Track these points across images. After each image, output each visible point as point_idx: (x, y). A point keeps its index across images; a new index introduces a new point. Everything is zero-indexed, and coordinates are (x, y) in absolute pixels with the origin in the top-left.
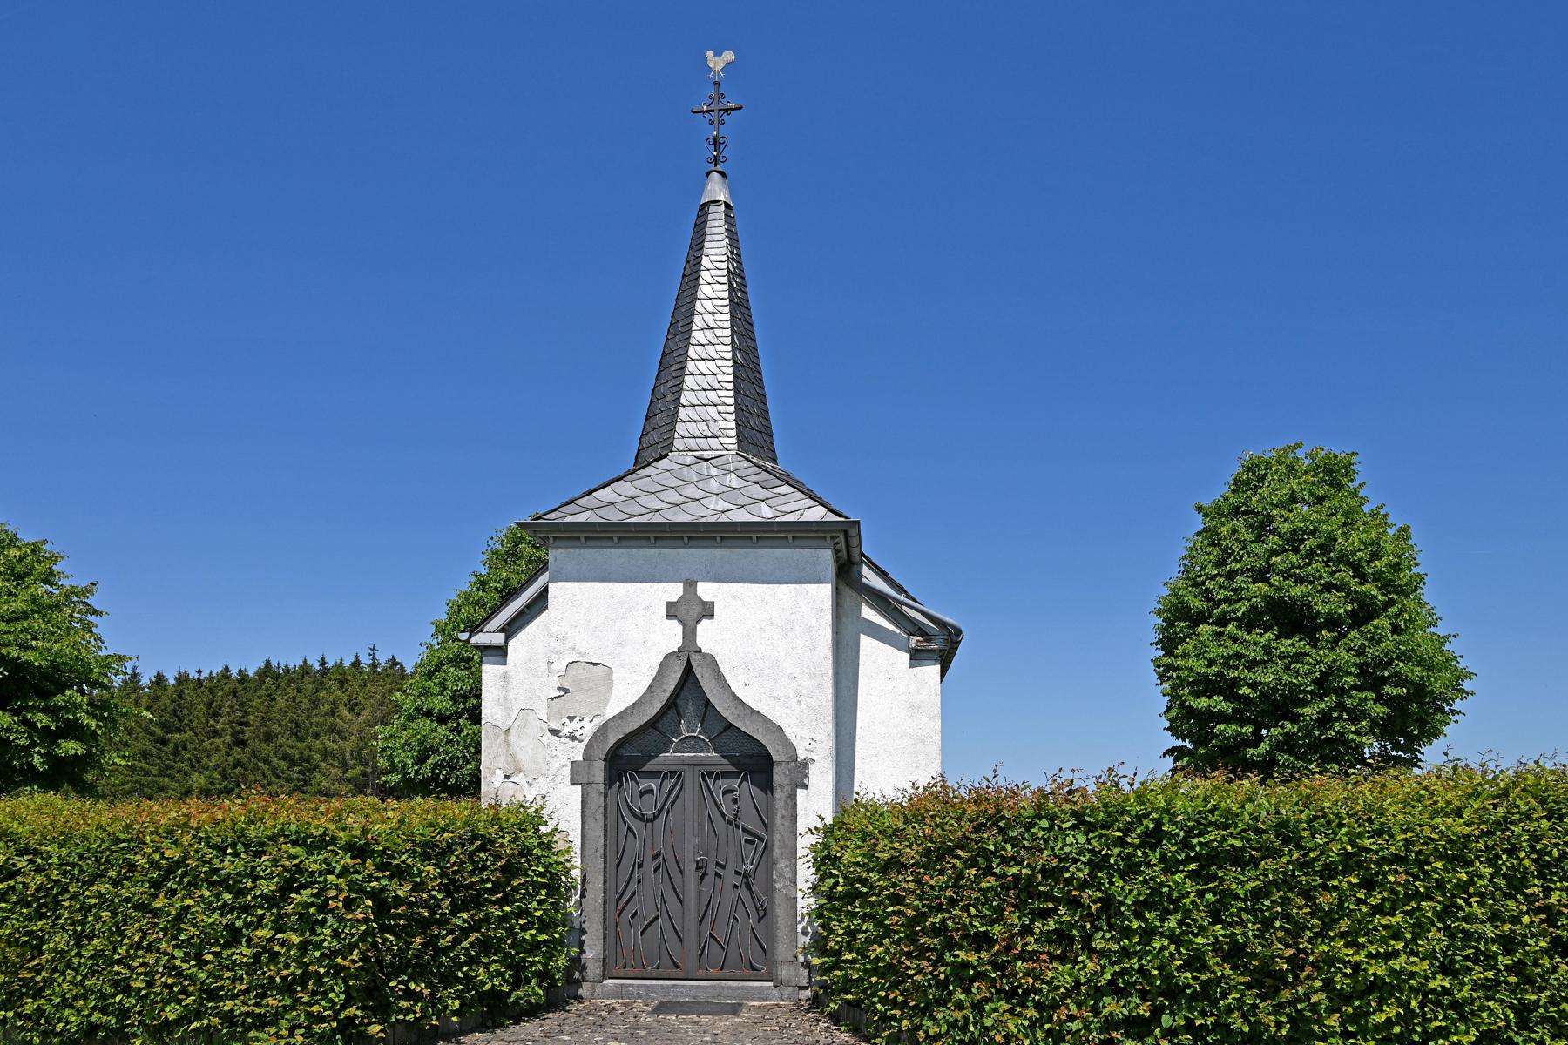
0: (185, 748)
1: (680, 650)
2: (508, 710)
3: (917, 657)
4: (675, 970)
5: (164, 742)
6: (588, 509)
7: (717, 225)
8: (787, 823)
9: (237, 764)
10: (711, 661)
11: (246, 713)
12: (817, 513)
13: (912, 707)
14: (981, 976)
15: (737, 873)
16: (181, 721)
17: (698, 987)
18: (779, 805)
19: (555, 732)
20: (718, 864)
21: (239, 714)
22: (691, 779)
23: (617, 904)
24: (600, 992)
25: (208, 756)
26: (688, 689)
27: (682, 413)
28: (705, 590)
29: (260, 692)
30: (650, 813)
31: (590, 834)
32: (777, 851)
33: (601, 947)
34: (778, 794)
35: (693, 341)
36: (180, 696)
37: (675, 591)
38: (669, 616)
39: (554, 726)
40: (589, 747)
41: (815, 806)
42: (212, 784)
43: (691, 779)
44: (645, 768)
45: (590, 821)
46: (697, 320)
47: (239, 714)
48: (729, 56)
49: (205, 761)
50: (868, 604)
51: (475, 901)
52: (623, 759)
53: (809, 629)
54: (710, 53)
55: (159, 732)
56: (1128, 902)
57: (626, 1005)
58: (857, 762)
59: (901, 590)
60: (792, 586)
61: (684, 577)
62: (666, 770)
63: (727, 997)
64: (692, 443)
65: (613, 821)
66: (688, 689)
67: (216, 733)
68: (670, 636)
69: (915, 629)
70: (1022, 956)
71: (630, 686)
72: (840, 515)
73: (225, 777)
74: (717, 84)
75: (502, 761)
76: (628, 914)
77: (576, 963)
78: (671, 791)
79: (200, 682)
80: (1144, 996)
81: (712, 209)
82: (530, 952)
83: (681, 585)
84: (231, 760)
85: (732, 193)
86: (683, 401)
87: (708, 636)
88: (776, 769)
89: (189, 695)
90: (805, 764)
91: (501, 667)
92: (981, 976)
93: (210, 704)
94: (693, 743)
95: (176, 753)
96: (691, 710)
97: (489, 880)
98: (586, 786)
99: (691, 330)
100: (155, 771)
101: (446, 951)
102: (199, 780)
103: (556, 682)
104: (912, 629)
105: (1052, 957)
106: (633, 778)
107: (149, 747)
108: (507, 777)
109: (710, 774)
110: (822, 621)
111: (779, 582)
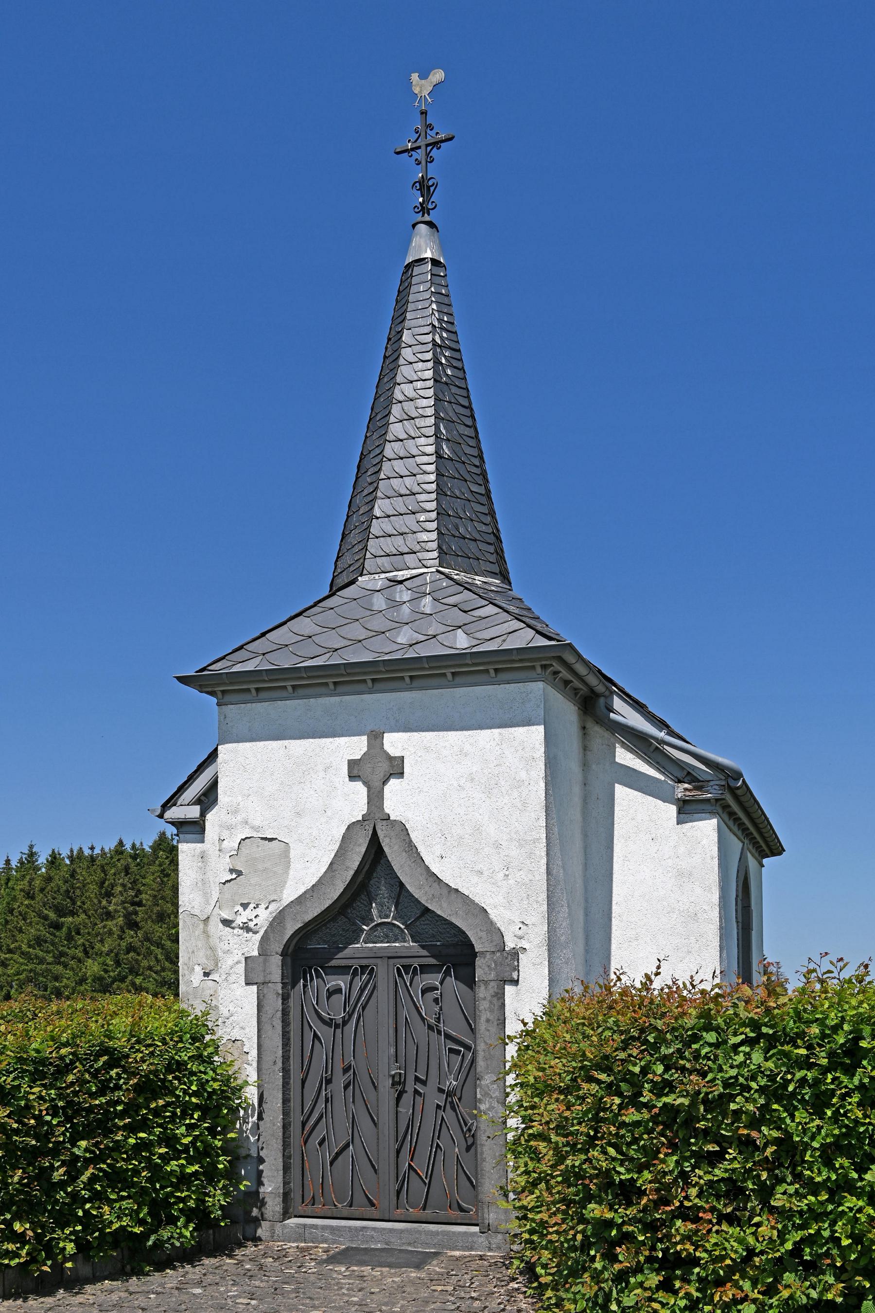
0: (78, 933)
1: (365, 818)
2: (206, 896)
3: (686, 810)
4: (370, 1209)
5: (57, 926)
6: (257, 654)
7: (422, 288)
8: (494, 1029)
9: (130, 949)
10: (402, 829)
11: (139, 892)
12: (524, 638)
13: (680, 874)
14: (627, 1238)
15: (441, 1091)
16: (74, 903)
17: (391, 1230)
18: (483, 1005)
19: (227, 923)
20: (417, 1079)
21: (132, 893)
22: (384, 974)
23: (299, 1129)
24: (282, 1232)
25: (102, 941)
26: (374, 867)
27: (375, 529)
28: (394, 743)
29: (153, 868)
30: (339, 1016)
31: (266, 1043)
32: (481, 1064)
33: (280, 1179)
34: (482, 992)
35: (390, 437)
36: (72, 876)
37: (356, 746)
38: (352, 777)
39: (226, 915)
40: (264, 940)
41: (526, 1002)
42: (106, 971)
43: (384, 974)
44: (333, 963)
45: (267, 1027)
46: (396, 410)
47: (132, 893)
48: (438, 75)
49: (98, 946)
50: (623, 745)
51: (102, 1125)
52: (306, 951)
53: (518, 784)
54: (415, 77)
55: (52, 915)
56: (816, 1145)
57: (302, 1250)
58: (614, 947)
59: (662, 724)
60: (496, 731)
61: (369, 728)
62: (355, 963)
63: (428, 1245)
64: (384, 562)
65: (290, 1032)
66: (374, 867)
67: (109, 915)
68: (354, 801)
69: (686, 775)
70: (684, 1213)
71: (310, 865)
72: (550, 638)
73: (118, 963)
74: (424, 113)
75: (201, 956)
76: (315, 1140)
77: (254, 1198)
78: (362, 990)
79: (92, 859)
80: (839, 1273)
81: (417, 270)
82: (177, 1187)
83: (365, 738)
84: (124, 944)
85: (443, 247)
86: (377, 512)
87: (397, 800)
88: (479, 962)
89: (82, 873)
90: (515, 954)
91: (199, 845)
92: (627, 1238)
93: (103, 883)
94: (388, 931)
95: (69, 938)
96: (383, 891)
97: (118, 1102)
98: (262, 985)
99: (388, 424)
100: (50, 959)
101: (62, 1185)
102: (92, 967)
103: (226, 862)
104: (680, 775)
105: (722, 1218)
106: (319, 975)
107: (44, 933)
108: (206, 974)
109: (407, 968)
110: (533, 774)
111: (481, 727)
